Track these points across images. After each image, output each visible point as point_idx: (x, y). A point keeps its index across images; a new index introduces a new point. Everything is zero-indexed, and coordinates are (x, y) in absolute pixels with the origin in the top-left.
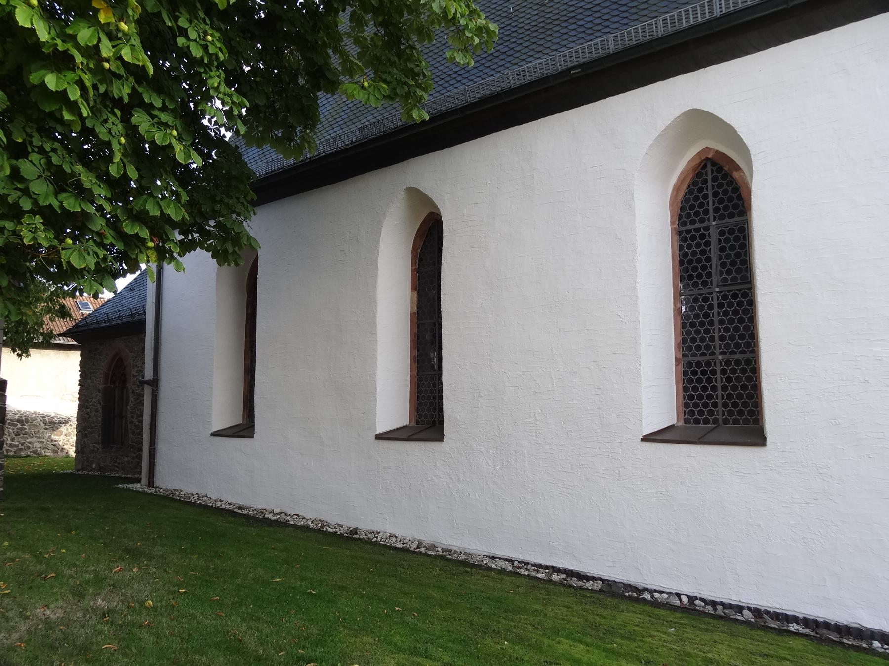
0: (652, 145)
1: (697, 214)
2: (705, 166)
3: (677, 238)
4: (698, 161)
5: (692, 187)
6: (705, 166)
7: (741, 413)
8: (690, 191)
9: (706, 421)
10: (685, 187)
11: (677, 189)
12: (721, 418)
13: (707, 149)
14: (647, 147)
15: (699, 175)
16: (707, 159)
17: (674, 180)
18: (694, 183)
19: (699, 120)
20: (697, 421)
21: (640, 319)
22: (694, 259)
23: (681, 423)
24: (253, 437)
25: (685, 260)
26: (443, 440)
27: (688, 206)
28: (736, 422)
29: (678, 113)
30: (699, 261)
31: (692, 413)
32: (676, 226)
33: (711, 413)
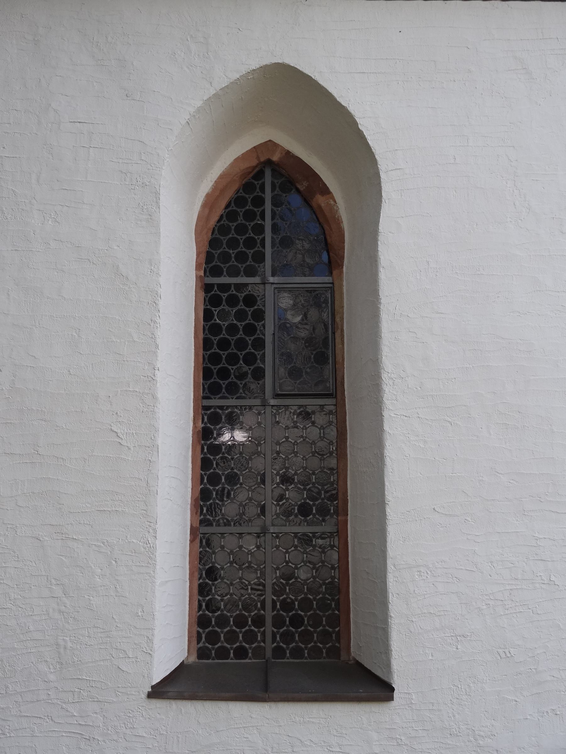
0: (199, 110)
1: (241, 258)
2: (260, 175)
3: (202, 294)
4: (254, 162)
5: (233, 207)
6: (260, 175)
7: (306, 636)
8: (230, 214)
9: (241, 653)
10: (223, 204)
11: (209, 203)
12: (269, 646)
13: (270, 145)
14: (192, 110)
15: (247, 187)
16: (269, 162)
17: (206, 186)
18: (238, 201)
19: (287, 88)
20: (223, 654)
21: (159, 442)
22: (233, 339)
23: (193, 658)
24: (376, 687)
25: (215, 340)
26: (391, 699)
27: (225, 240)
28: (297, 653)
29: (255, 63)
30: (241, 344)
31: (213, 638)
32: (202, 273)
33: (250, 637)
